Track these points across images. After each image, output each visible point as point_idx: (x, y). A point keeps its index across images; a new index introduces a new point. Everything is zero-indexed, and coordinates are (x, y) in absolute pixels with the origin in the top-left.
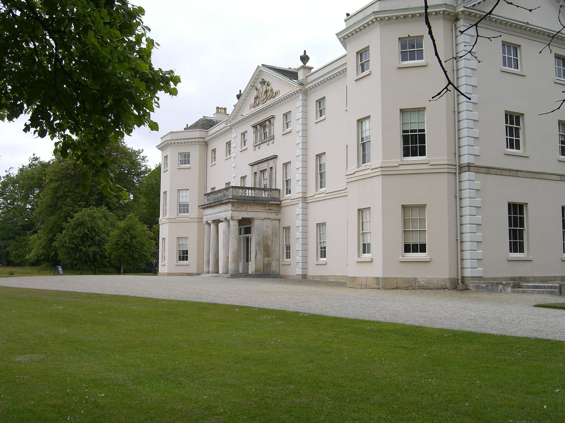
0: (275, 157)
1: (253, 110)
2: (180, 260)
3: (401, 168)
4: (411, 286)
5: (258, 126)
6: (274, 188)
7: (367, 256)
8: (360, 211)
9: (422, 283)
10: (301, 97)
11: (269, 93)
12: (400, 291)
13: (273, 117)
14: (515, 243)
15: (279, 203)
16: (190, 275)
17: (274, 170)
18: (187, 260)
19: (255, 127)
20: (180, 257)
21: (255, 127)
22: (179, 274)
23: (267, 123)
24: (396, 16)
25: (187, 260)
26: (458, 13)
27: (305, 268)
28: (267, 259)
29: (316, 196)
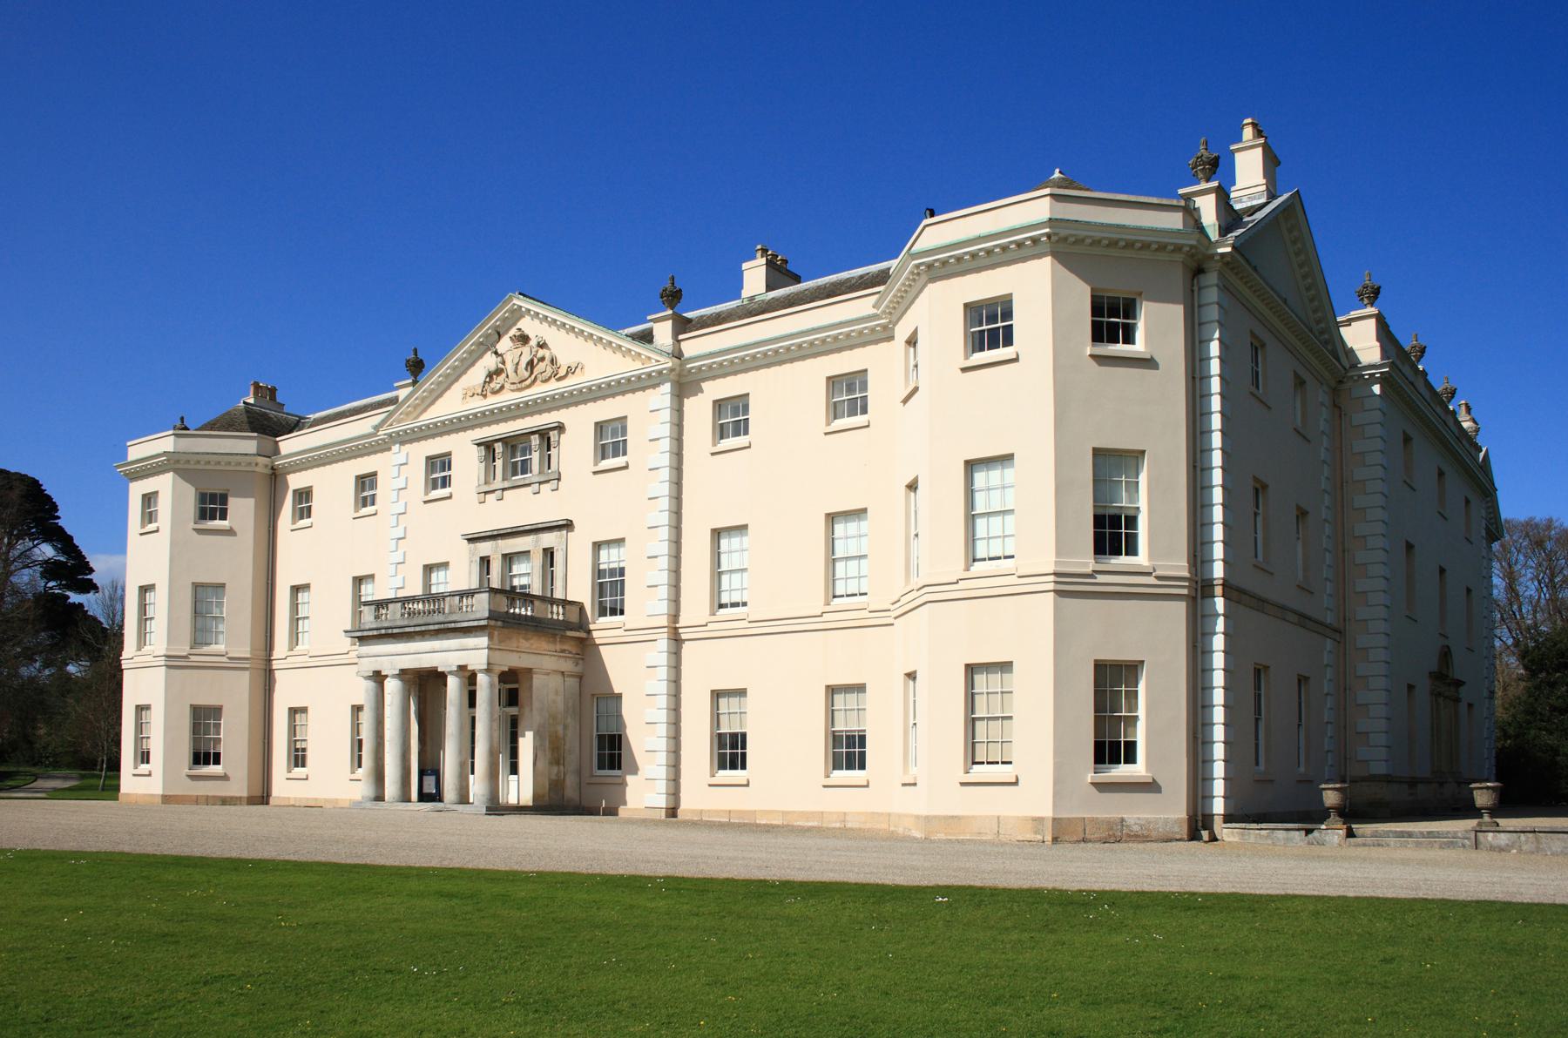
0: (568, 526)
1: (478, 404)
2: (722, 766)
3: (1101, 579)
4: (1116, 835)
5: (499, 447)
6: (558, 595)
7: (144, 768)
8: (1257, 672)
9: (1136, 828)
10: (667, 387)
11: (540, 367)
12: (1090, 845)
13: (560, 428)
14: (612, 747)
15: (583, 635)
16: (225, 801)
17: (558, 558)
18: (862, 767)
19: (488, 446)
20: (722, 758)
21: (488, 446)
22: (196, 800)
23: (535, 440)
24: (1031, 238)
25: (862, 767)
26: (1212, 256)
27: (675, 792)
28: (555, 769)
29: (711, 626)
